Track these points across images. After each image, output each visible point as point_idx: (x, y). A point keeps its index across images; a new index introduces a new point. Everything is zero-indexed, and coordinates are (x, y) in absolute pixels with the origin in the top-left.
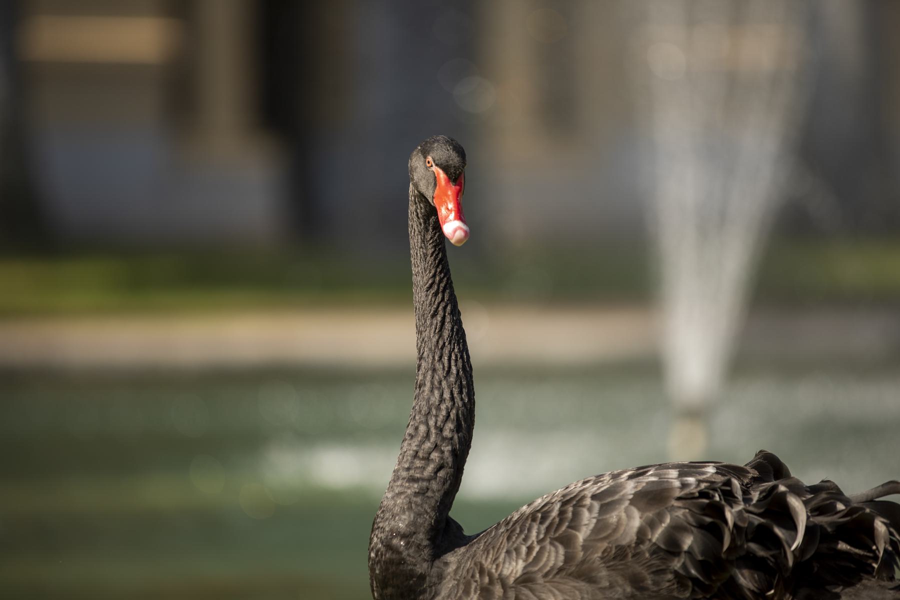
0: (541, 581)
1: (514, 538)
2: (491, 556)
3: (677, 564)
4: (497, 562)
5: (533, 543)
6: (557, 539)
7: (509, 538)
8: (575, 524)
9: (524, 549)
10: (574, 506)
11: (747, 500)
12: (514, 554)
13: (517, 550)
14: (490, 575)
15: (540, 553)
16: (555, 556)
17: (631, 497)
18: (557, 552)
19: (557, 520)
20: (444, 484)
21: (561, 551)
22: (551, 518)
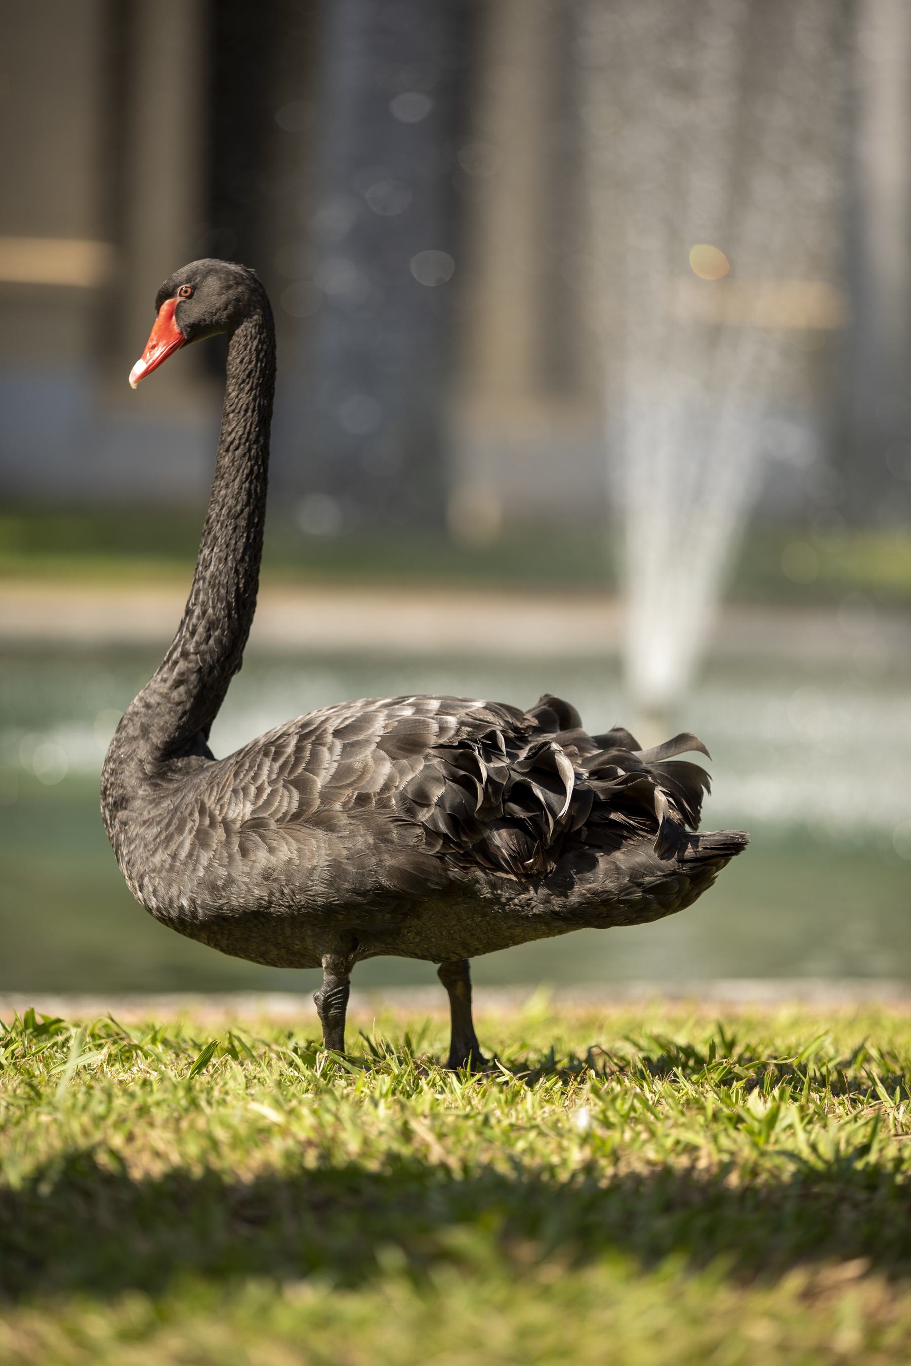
0: (273, 825)
1: (242, 776)
2: (214, 793)
3: (424, 816)
4: (221, 802)
5: (263, 783)
6: (292, 782)
7: (236, 775)
8: (314, 764)
9: (253, 790)
10: (313, 743)
11: (513, 756)
12: (242, 794)
13: (245, 789)
14: (212, 817)
15: (273, 793)
16: (288, 801)
17: (378, 739)
18: (290, 797)
19: (293, 759)
20: (181, 718)
21: (296, 795)
22: (286, 756)
